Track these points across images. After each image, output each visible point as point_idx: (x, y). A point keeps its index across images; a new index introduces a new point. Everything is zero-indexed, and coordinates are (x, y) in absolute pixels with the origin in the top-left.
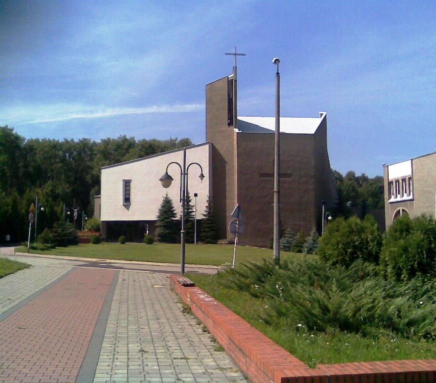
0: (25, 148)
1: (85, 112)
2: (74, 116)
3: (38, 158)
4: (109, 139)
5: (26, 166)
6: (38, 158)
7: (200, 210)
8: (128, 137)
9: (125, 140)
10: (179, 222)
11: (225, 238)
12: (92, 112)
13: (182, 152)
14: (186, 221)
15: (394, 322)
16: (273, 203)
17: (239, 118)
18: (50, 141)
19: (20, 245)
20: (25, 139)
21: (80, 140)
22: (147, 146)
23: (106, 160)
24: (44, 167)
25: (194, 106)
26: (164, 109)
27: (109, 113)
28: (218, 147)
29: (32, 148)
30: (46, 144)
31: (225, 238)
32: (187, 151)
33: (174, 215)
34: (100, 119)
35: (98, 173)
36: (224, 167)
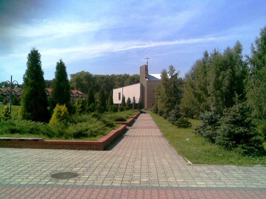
0: (93, 78)
1: (139, 45)
2: (135, 47)
3: (98, 81)
4: (121, 75)
5: (94, 84)
6: (98, 81)
7: (137, 101)
8: (127, 74)
9: (126, 75)
10: (132, 104)
11: (144, 108)
12: (144, 45)
13: (122, 88)
14: (134, 104)
15: (159, 129)
16: (134, 106)
17: (149, 74)
18: (101, 75)
19: (52, 116)
20: (93, 75)
21: (111, 75)
22: (132, 78)
23: (119, 82)
24: (99, 85)
25: (200, 39)
26: (182, 42)
27: (153, 45)
28: (143, 84)
29: (96, 77)
30: (100, 77)
31: (144, 108)
32: (123, 88)
33: (131, 102)
34: (148, 48)
35: (116, 86)
36: (144, 89)
